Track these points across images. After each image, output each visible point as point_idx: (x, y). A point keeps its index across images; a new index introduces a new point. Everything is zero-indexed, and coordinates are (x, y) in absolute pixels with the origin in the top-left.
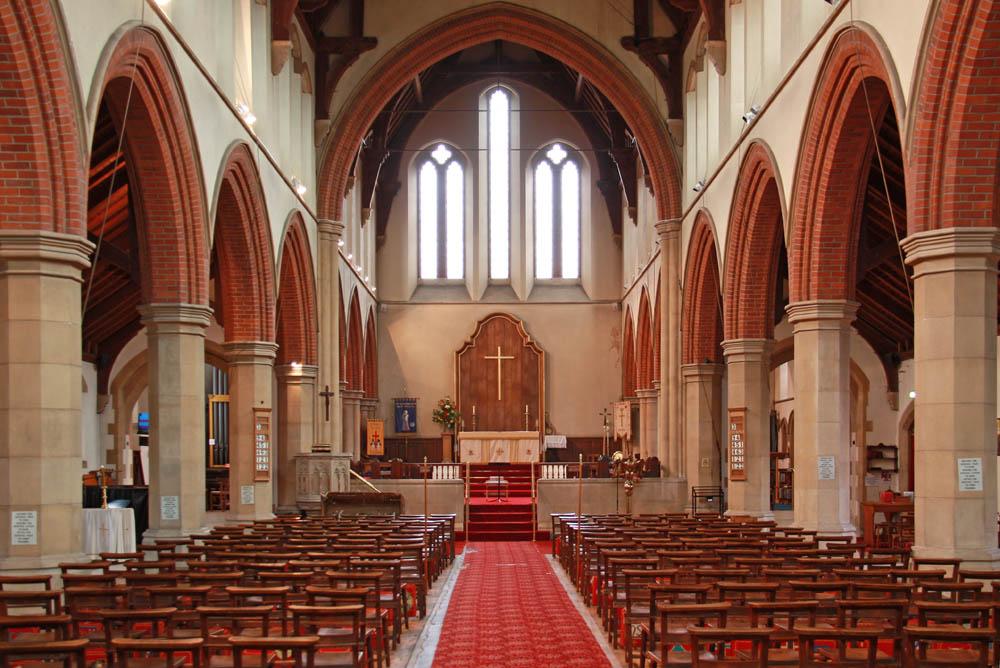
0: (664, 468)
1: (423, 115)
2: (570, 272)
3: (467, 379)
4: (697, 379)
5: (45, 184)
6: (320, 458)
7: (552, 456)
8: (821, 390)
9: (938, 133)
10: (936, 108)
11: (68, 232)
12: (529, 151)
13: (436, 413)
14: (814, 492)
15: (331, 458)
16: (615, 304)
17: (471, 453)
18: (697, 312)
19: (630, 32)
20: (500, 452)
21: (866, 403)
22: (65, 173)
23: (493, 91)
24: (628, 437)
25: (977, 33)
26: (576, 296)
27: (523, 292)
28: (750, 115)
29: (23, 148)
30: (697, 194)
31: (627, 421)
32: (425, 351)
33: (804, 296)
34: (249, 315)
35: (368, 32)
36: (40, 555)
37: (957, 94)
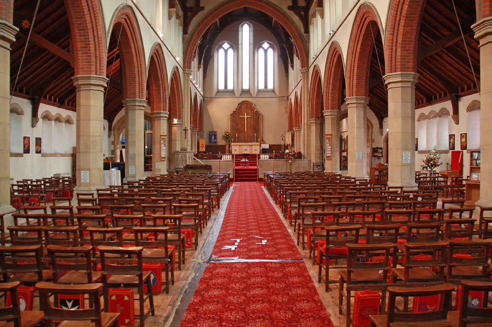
1: (220, 33)
2: (270, 86)
5: (93, 59)
7: (264, 151)
8: (357, 128)
11: (100, 75)
12: (256, 44)
13: (223, 136)
15: (187, 152)
16: (286, 98)
17: (236, 150)
19: (291, 4)
20: (246, 150)
21: (372, 133)
22: (100, 55)
23: (244, 24)
26: (272, 95)
27: (254, 94)
29: (87, 47)
30: (314, 59)
31: (290, 139)
32: (220, 115)
34: (159, 102)
35: (201, 5)
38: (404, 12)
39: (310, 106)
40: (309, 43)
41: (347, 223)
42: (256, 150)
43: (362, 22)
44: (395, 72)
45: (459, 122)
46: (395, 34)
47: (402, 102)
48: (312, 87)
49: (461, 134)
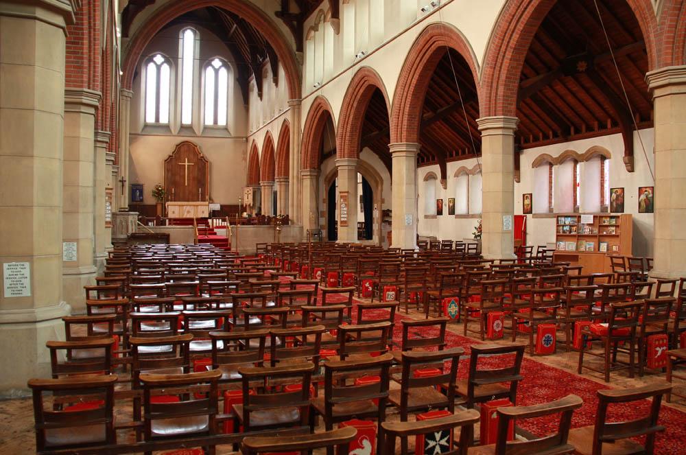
0: (291, 221)
2: (222, 122)
3: (170, 174)
4: (309, 177)
6: (122, 215)
7: (214, 214)
8: (406, 184)
9: (496, 76)
10: (495, 64)
11: (94, 89)
12: (204, 60)
14: (403, 231)
16: (245, 139)
17: (174, 212)
18: (310, 145)
19: (279, 9)
20: (188, 212)
21: (382, 190)
23: (186, 30)
24: (251, 205)
25: (516, 36)
26: (224, 134)
27: (198, 131)
28: (360, 54)
29: (78, 43)
30: (315, 89)
31: (251, 197)
32: (149, 158)
33: (399, 140)
36: (78, 267)
37: (505, 60)
38: (513, 43)
39: (303, 152)
40: (302, 65)
41: (327, 311)
42: (203, 212)
43: (427, 47)
44: (495, 115)
45: (521, 179)
46: (497, 68)
47: (503, 153)
48: (307, 126)
49: (524, 195)
